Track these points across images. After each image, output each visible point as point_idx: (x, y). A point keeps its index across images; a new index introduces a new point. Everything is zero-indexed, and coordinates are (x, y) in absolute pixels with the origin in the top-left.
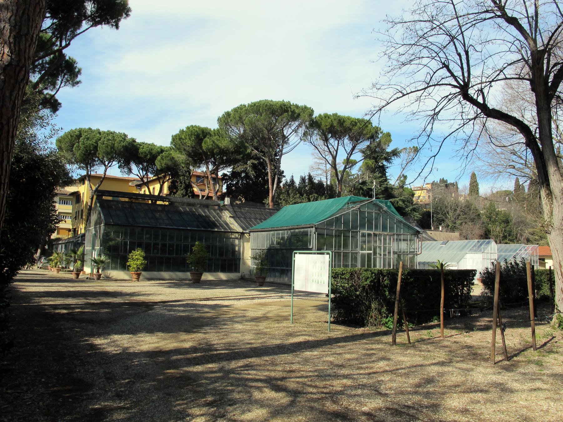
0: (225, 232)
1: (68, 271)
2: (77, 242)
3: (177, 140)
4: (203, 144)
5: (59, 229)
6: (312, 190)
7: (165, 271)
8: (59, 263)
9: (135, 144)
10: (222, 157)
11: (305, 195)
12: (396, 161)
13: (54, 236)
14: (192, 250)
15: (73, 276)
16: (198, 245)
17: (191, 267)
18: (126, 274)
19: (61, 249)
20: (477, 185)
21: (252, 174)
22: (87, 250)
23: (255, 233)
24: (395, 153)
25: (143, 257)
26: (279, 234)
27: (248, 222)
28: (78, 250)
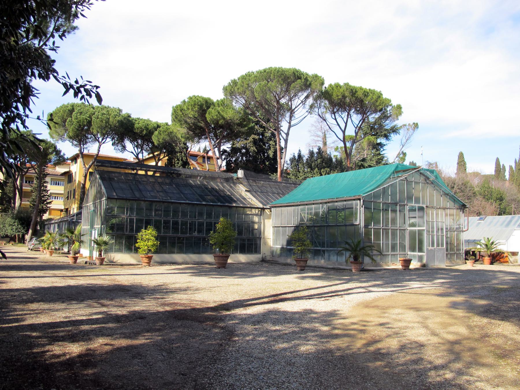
0: (244, 207)
1: (62, 253)
2: (71, 223)
3: (178, 113)
4: (207, 115)
5: (51, 210)
6: (321, 163)
7: (177, 253)
8: (52, 245)
9: (130, 119)
10: (224, 130)
11: (316, 169)
13: (46, 216)
14: (215, 227)
15: (69, 260)
16: (223, 221)
17: (216, 248)
18: (132, 256)
19: (54, 229)
20: (465, 164)
21: (253, 149)
22: (84, 229)
23: (278, 209)
24: (394, 130)
25: (155, 237)
27: (267, 198)
28: (75, 229)
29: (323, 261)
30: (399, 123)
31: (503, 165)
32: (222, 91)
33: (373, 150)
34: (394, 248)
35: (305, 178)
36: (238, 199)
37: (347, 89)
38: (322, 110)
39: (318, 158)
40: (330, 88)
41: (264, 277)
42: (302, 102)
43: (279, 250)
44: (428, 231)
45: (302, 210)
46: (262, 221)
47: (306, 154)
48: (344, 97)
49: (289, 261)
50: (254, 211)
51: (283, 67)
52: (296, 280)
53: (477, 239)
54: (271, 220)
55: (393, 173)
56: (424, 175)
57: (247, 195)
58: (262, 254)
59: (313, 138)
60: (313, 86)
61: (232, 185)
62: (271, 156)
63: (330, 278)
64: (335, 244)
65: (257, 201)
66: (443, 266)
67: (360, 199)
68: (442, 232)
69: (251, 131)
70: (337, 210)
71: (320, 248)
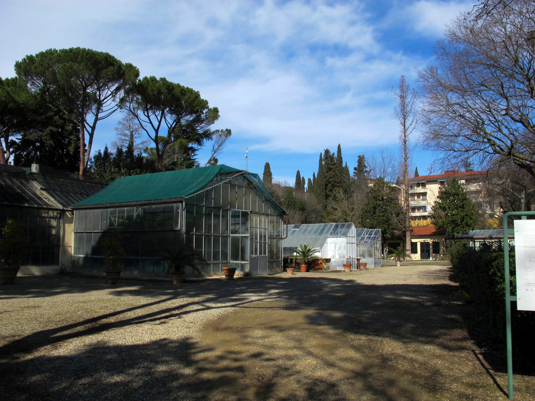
12: (208, 144)
20: (271, 174)
23: (81, 212)
24: (207, 135)
26: (123, 212)
27: (67, 197)
29: (136, 272)
30: (213, 128)
31: (303, 177)
32: (13, 68)
33: (183, 154)
34: (216, 257)
35: (113, 179)
36: (31, 198)
37: (164, 85)
38: (133, 105)
39: (127, 157)
40: (145, 81)
41: (69, 295)
42: (112, 93)
43: (81, 260)
44: (252, 239)
45: (111, 213)
46: (62, 225)
47: (113, 151)
48: (160, 93)
49: (95, 272)
50: (51, 213)
51: (94, 50)
52: (111, 296)
53: (293, 246)
54: (73, 225)
55: (217, 175)
56: (248, 179)
57: (42, 194)
58: (60, 265)
59: (120, 136)
60: (127, 77)
61: (23, 181)
62: (71, 153)
63: (152, 292)
64: (158, 251)
65: (55, 202)
66: (265, 275)
67: (182, 202)
68: (265, 240)
69: (49, 121)
70: (154, 213)
71: (132, 257)
